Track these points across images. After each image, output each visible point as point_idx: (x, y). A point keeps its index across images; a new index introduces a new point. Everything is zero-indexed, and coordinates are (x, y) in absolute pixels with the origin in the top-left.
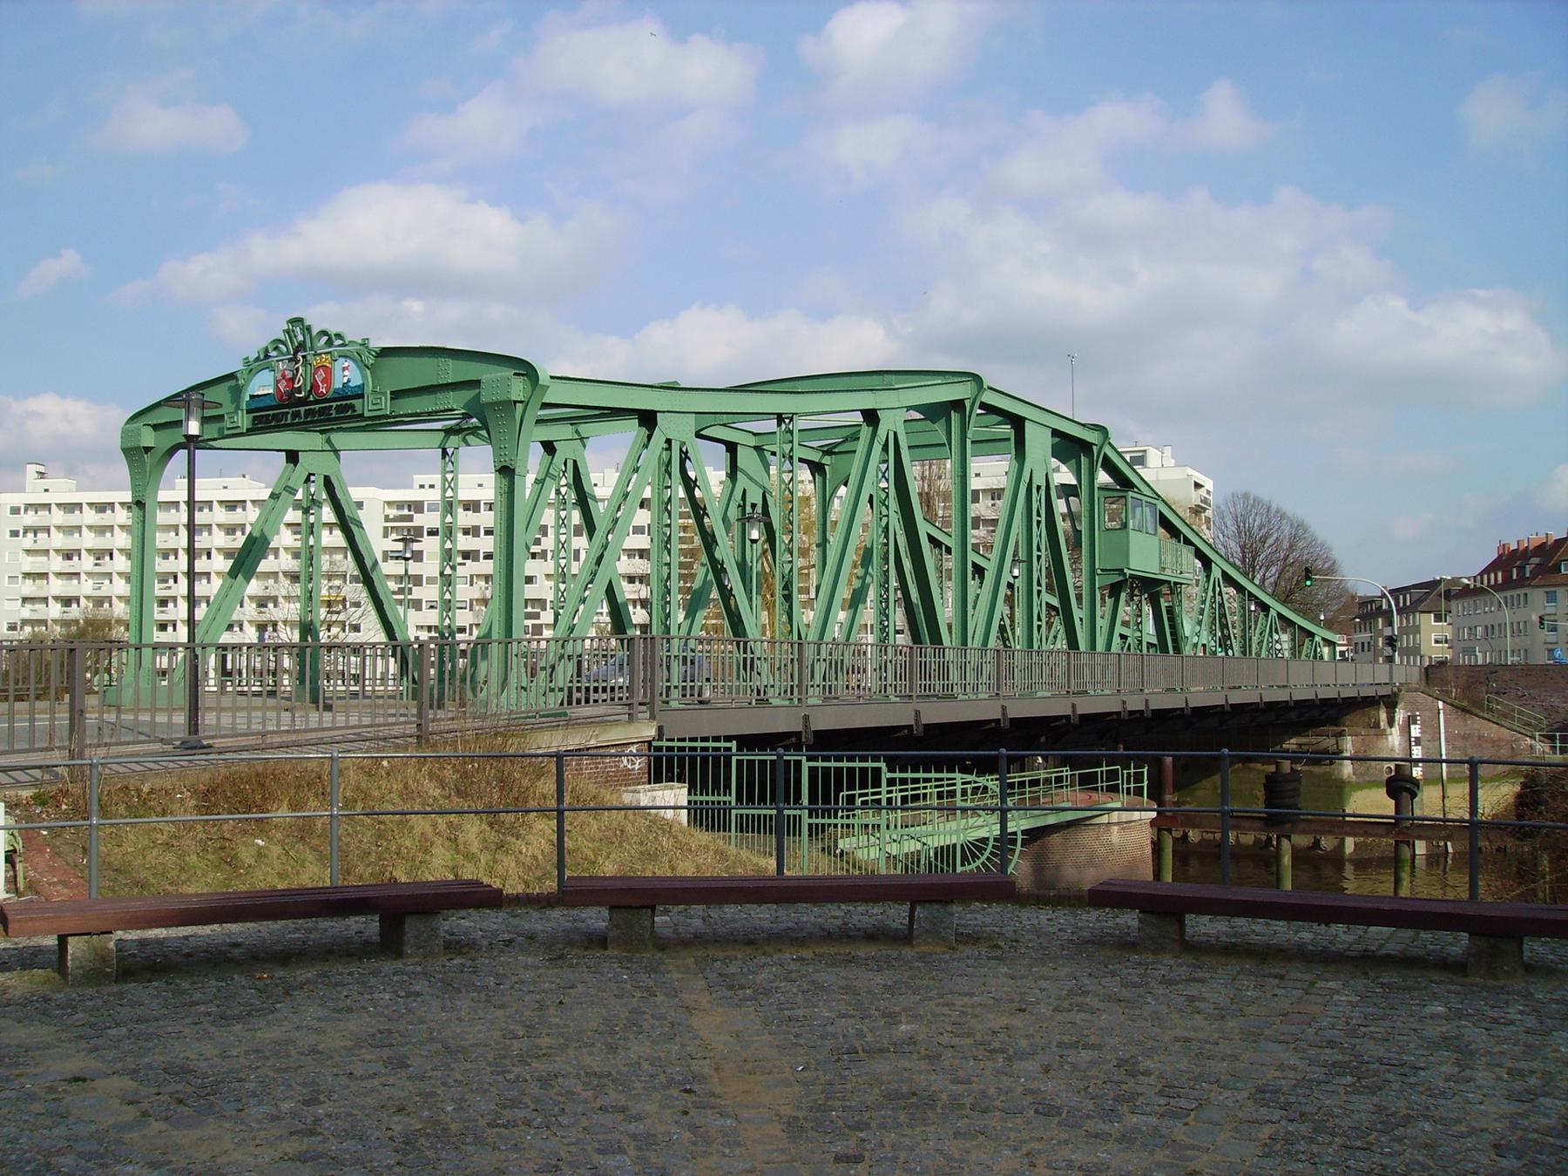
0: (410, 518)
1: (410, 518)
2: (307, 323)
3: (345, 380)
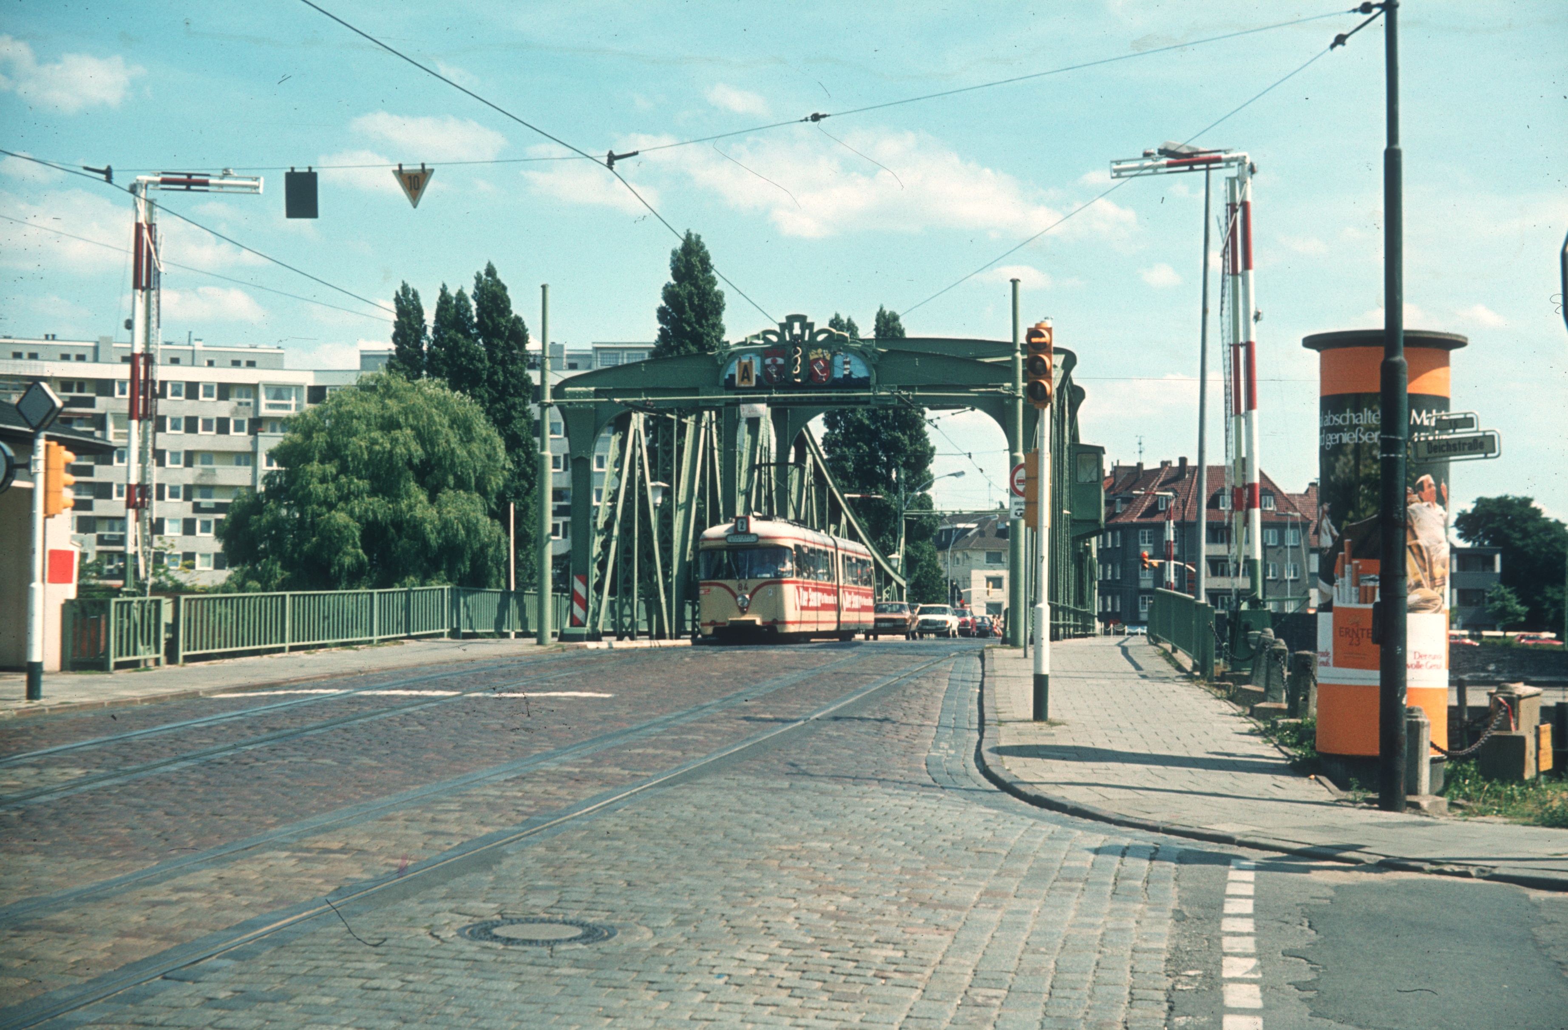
0: (90, 403)
1: (90, 403)
2: (809, 320)
3: (846, 372)
